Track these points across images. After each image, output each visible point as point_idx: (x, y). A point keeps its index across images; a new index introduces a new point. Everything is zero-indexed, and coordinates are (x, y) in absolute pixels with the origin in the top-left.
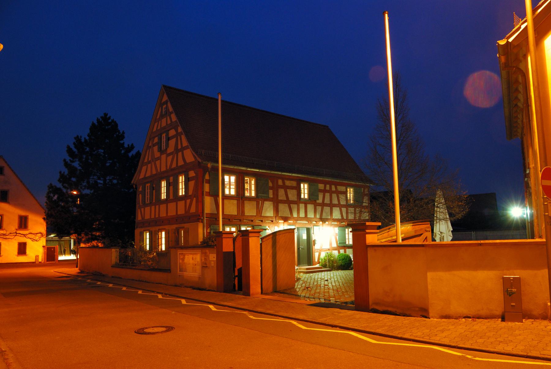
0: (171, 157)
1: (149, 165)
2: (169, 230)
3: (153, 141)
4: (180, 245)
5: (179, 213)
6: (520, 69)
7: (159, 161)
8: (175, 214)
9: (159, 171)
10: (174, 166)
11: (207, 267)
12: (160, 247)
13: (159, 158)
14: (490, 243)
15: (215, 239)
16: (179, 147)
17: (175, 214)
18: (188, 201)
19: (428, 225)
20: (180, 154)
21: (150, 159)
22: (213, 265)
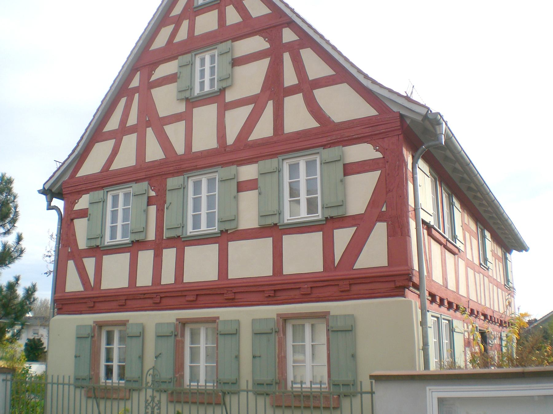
3: (150, 75)
8: (269, 272)
17: (269, 272)
21: (132, 120)
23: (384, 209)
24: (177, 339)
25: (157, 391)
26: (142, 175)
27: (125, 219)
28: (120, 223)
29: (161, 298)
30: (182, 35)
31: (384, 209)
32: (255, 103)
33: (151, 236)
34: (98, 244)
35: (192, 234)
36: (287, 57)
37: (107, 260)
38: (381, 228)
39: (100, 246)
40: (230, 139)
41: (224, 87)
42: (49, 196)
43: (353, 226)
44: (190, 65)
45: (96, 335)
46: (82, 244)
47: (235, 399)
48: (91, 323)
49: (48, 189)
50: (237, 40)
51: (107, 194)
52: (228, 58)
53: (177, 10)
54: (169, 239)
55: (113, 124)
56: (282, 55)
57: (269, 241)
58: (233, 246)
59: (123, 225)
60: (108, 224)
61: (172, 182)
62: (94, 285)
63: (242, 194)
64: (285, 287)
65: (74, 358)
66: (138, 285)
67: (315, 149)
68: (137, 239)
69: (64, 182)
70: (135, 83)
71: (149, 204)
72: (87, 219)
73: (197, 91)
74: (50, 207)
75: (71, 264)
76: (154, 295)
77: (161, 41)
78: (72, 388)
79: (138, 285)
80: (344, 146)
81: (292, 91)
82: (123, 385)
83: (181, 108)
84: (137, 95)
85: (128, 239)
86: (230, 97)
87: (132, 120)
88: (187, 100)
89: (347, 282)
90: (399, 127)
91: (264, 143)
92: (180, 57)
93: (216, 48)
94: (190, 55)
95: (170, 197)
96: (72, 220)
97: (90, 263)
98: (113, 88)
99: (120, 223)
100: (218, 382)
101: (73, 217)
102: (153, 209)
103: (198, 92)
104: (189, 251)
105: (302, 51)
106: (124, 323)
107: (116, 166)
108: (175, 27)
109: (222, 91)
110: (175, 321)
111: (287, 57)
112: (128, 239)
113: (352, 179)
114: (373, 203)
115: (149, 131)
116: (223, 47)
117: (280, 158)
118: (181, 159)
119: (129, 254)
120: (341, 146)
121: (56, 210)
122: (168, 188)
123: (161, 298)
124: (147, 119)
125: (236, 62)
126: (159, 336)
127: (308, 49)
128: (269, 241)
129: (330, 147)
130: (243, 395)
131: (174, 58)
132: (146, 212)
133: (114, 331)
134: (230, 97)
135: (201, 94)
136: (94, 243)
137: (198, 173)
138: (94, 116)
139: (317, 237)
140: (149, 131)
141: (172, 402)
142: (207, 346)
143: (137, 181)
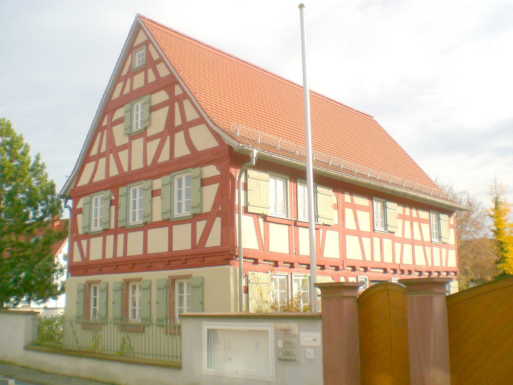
0: (156, 143)
1: (209, 210)
2: (151, 281)
3: (112, 117)
4: (129, 322)
5: (176, 248)
6: (345, 286)
7: (127, 150)
8: (166, 250)
9: (126, 169)
10: (164, 157)
11: (292, 360)
12: (422, 267)
13: (127, 147)
14: (237, 287)
15: (58, 323)
16: (178, 122)
17: (166, 250)
18: (201, 225)
19: (360, 277)
20: (180, 136)
21: (103, 149)
22: (312, 356)
23: (220, 209)
24: (123, 292)
25: (159, 326)
26: (108, 186)
27: (188, 196)
28: (184, 200)
29: (117, 266)
30: (127, 91)
31: (220, 209)
32: (161, 137)
33: (113, 226)
34: (124, 225)
35: (132, 224)
36: (177, 105)
37: (176, 228)
38: (218, 221)
39: (170, 219)
40: (149, 163)
41: (146, 126)
42: (65, 199)
43: (205, 220)
44: (130, 111)
45: (87, 289)
46: (81, 232)
47: (106, 326)
48: (167, 277)
49: (63, 195)
50: (153, 94)
51: (92, 198)
52: (147, 107)
53: (125, 72)
54: (121, 228)
55: (94, 152)
56: (174, 104)
57: (166, 229)
58: (150, 232)
59: (186, 201)
60: (131, 211)
61: (122, 190)
62: (199, 243)
63: (154, 198)
64: (176, 258)
65: (156, 304)
66: (148, 253)
67: (97, 194)
68: (195, 213)
69: (72, 190)
70: (105, 123)
71: (111, 205)
72: (160, 197)
73: (134, 129)
74: (66, 206)
75: (76, 243)
76: (114, 264)
77: (116, 95)
78: (112, 325)
79: (148, 253)
80: (202, 167)
81: (179, 129)
82: (140, 323)
83: (126, 140)
84: (105, 131)
85: (189, 212)
86: (150, 133)
87: (103, 149)
88: (129, 135)
89: (202, 256)
90: (228, 155)
91: (165, 164)
92: (125, 105)
93: (143, 99)
94: (130, 104)
95: (122, 201)
96: (76, 215)
97: (84, 243)
98: (93, 127)
99: (184, 200)
100: (143, 320)
101: (76, 213)
102: (113, 207)
103: (135, 129)
104: (130, 235)
105: (184, 101)
106: (189, 277)
107: (95, 180)
108: (124, 83)
109: (146, 129)
110: (167, 278)
111: (177, 105)
112: (189, 212)
113: (206, 188)
114: (215, 206)
115: (111, 155)
116: (146, 98)
117: (173, 174)
118: (126, 175)
119: (190, 224)
120: (199, 168)
121: (69, 208)
122: (120, 195)
123: (151, 263)
124: (110, 148)
125: (152, 109)
126: (115, 290)
127: (114, 131)
128: (166, 229)
129: (196, 167)
130: (109, 325)
131: (122, 106)
132: (110, 210)
133: (183, 283)
134: (150, 133)
135: (137, 131)
136: (166, 216)
137: (138, 183)
138: (84, 146)
139: (189, 226)
140: (111, 155)
141: (85, 329)
142: (188, 295)
143: (106, 189)
